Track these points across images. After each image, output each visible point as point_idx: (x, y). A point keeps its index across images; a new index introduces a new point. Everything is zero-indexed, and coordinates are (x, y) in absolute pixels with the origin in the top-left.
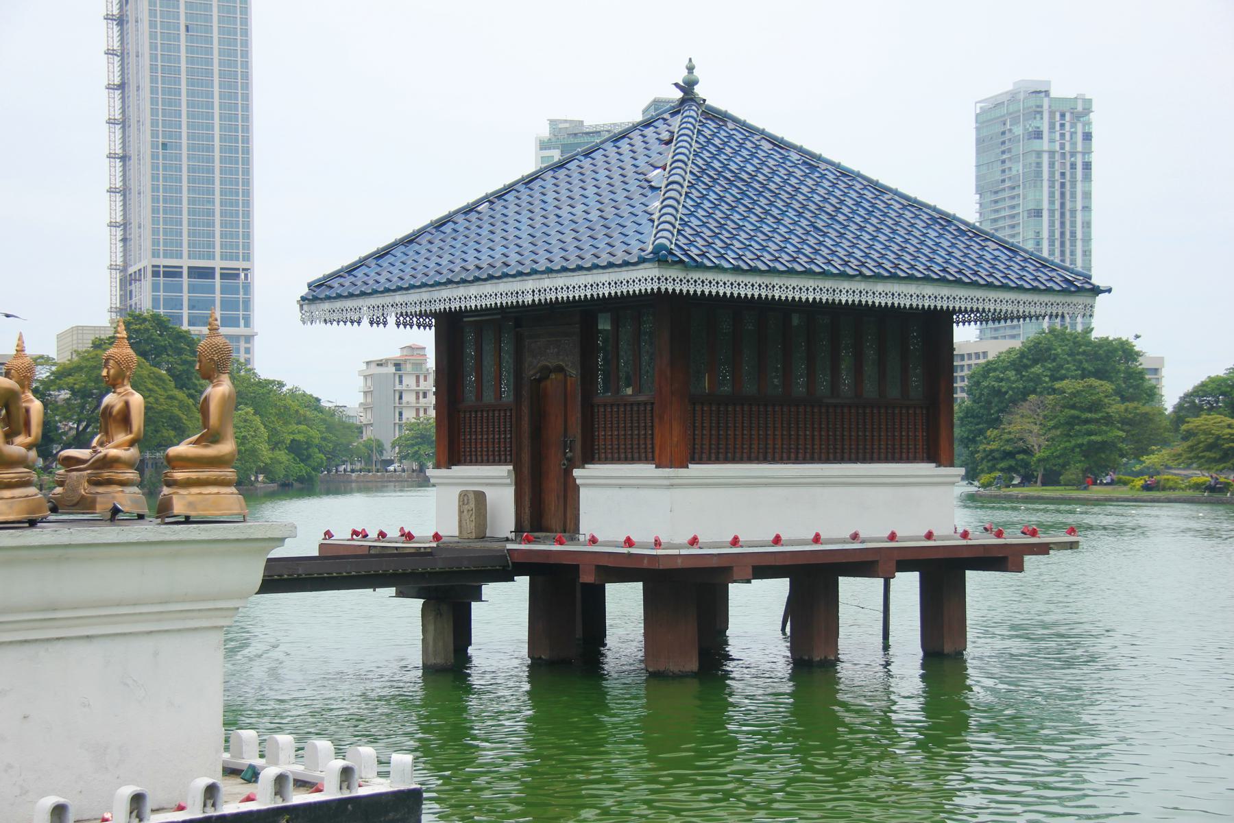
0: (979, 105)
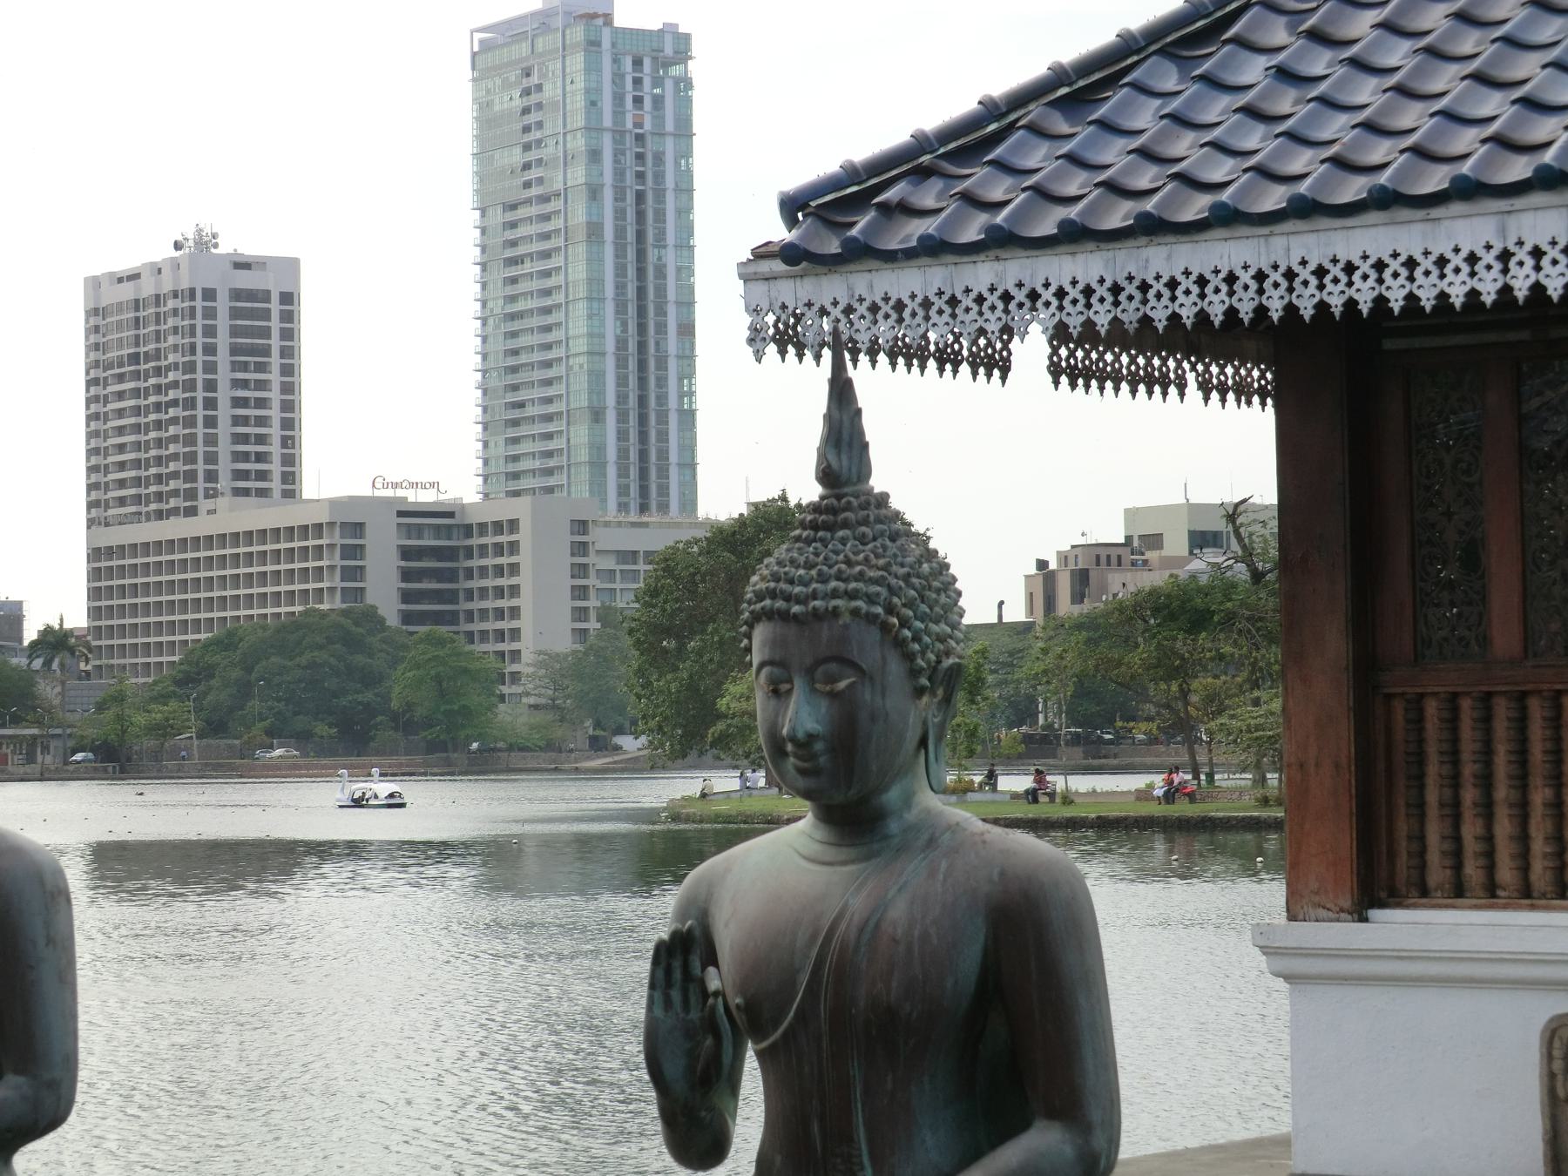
0: (477, 36)
